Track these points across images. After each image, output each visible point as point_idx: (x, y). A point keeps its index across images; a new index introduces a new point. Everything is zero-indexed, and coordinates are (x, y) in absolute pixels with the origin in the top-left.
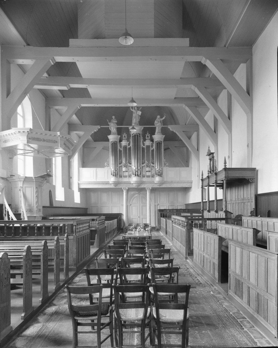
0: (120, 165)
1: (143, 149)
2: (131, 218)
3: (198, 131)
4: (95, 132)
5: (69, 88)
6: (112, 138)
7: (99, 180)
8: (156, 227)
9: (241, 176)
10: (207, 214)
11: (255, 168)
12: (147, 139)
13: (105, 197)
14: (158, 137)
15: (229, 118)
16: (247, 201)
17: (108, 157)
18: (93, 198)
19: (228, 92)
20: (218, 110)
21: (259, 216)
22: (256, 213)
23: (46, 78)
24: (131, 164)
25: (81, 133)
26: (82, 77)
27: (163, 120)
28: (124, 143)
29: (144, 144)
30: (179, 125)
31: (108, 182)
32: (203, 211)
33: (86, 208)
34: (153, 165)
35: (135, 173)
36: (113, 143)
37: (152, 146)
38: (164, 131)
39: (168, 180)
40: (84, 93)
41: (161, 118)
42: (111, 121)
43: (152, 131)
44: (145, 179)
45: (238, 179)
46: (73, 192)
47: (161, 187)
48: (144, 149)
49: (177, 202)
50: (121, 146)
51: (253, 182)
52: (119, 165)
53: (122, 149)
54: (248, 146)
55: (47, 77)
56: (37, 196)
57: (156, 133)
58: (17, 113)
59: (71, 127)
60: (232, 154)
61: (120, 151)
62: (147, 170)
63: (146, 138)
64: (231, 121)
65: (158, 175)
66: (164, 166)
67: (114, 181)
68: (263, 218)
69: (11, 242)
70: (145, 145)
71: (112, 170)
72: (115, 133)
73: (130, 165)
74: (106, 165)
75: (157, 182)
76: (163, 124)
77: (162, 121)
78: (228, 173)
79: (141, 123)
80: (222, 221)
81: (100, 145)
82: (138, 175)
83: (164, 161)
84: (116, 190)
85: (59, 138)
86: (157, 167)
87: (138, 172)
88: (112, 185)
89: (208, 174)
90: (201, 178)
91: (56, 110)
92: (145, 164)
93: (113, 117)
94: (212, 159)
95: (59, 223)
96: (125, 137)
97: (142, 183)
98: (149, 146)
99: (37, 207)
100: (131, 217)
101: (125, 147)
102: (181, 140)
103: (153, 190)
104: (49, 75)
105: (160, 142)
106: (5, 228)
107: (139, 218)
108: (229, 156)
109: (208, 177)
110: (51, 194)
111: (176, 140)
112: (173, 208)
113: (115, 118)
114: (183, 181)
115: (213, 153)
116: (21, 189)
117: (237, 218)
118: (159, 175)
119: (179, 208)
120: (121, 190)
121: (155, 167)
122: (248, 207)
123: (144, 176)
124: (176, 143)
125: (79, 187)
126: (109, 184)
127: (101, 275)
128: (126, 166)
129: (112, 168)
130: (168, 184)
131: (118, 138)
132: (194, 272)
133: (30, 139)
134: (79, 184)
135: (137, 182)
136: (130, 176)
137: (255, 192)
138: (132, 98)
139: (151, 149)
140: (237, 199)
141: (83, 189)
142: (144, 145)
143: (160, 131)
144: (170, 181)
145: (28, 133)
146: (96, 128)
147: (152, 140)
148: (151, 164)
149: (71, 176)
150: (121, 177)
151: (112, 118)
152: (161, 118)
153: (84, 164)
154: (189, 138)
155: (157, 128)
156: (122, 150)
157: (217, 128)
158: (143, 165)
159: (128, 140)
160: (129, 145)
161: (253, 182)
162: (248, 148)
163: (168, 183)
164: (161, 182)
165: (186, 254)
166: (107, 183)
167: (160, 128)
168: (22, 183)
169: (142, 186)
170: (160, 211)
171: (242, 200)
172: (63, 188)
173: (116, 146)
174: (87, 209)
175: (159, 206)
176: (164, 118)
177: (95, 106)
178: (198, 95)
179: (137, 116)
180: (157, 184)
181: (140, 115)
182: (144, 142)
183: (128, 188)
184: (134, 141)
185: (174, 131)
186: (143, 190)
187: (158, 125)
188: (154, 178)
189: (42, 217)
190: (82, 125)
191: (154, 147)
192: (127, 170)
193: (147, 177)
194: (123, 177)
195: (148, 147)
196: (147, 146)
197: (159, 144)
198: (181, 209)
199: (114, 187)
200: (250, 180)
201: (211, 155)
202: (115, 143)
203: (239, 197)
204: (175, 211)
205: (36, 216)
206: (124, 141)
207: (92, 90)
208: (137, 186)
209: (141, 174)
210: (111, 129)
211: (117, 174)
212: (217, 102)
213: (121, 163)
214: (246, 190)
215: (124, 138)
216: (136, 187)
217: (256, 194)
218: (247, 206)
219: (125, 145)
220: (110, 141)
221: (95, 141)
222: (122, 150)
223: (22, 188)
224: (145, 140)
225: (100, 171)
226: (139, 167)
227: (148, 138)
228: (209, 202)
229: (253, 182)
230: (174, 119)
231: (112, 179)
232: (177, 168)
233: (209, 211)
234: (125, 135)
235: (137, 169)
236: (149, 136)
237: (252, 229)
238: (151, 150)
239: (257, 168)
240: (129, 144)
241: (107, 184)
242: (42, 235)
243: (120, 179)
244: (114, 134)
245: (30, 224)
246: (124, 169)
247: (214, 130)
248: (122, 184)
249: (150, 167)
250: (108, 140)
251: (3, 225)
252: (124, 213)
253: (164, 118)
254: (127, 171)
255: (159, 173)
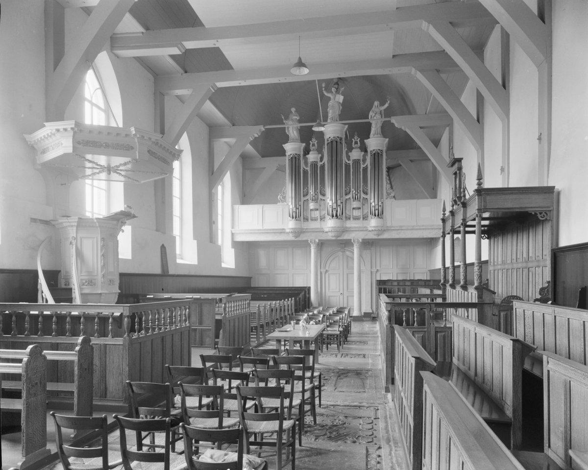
0: (306, 198)
1: (347, 166)
2: (327, 298)
3: (450, 124)
4: (256, 138)
5: (184, 51)
6: (291, 148)
7: (268, 226)
8: (373, 313)
9: (517, 206)
10: (452, 291)
11: (554, 187)
12: (355, 148)
13: (281, 258)
14: (375, 142)
15: (505, 85)
16: (535, 264)
17: (284, 184)
18: (263, 259)
19: (502, 26)
20: (485, 75)
21: (550, 302)
22: (554, 294)
23: (141, 35)
24: (324, 195)
25: (232, 141)
26: (204, 26)
27: (385, 110)
28: (312, 157)
29: (348, 158)
30: (417, 114)
31: (283, 229)
32: (444, 285)
33: (248, 276)
34: (365, 196)
35: (332, 211)
36: (292, 158)
37: (364, 160)
38: (387, 130)
39: (393, 225)
40: (215, 61)
41: (380, 106)
42: (288, 117)
43: (364, 131)
44: (351, 224)
45: (516, 216)
46: (219, 250)
47: (379, 237)
48: (350, 166)
49: (293, 267)
50: (306, 163)
51: (548, 218)
52: (303, 199)
53: (308, 169)
54: (540, 139)
55: (143, 33)
56: (103, 255)
57: (371, 135)
58: (82, 99)
59: (214, 131)
60: (503, 161)
61: (305, 172)
62: (355, 206)
63: (353, 146)
64: (509, 90)
65: (375, 216)
66: (387, 199)
67: (293, 227)
68: (557, 309)
69: (4, 352)
70: (352, 159)
71: (291, 207)
72: (297, 140)
73: (323, 198)
74: (280, 198)
75: (373, 229)
76: (384, 116)
77: (383, 112)
78: (485, 201)
79: (342, 117)
80: (470, 309)
81: (271, 164)
82: (336, 215)
83: (386, 189)
84: (298, 244)
85: (136, 140)
86: (373, 202)
87: (337, 211)
88: (291, 234)
89: (453, 206)
90: (442, 216)
91: (177, 96)
92: (350, 196)
93: (293, 110)
94: (458, 172)
95: (113, 311)
96: (313, 145)
97: (345, 230)
98: (359, 160)
99: (103, 276)
100: (328, 294)
101: (314, 165)
102: (420, 148)
103: (367, 244)
104: (147, 29)
105: (379, 151)
106: (14, 318)
107: (341, 297)
108: (502, 167)
109: (452, 213)
110: (166, 253)
111: (412, 149)
112: (405, 279)
113: (295, 112)
114: (423, 226)
115: (459, 160)
116: (74, 242)
117: (504, 303)
118: (377, 215)
119: (416, 278)
120: (306, 245)
121: (369, 200)
122: (537, 279)
123: (348, 218)
124: (413, 154)
125: (233, 238)
126: (284, 232)
127: (266, 399)
128: (315, 200)
129: (290, 204)
130: (394, 232)
131: (302, 148)
132: (384, 431)
133: (79, 143)
134: (233, 234)
135: (334, 229)
136: (322, 218)
137: (552, 244)
138: (300, 59)
139: (362, 166)
140: (515, 261)
141: (243, 243)
142: (349, 160)
143: (379, 130)
144: (397, 227)
145: (75, 133)
146: (257, 131)
147: (364, 149)
148: (363, 195)
149: (214, 219)
150: (306, 219)
151: (291, 112)
152: (380, 106)
153: (245, 196)
154: (436, 143)
155: (373, 125)
156: (309, 171)
157: (483, 113)
158: (347, 197)
159: (320, 150)
160: (321, 161)
161: (546, 219)
162: (540, 143)
163: (393, 230)
164: (380, 228)
165: (387, 380)
166: (282, 231)
167: (380, 125)
168: (75, 231)
169: (346, 237)
170: (381, 283)
171: (526, 262)
172: (196, 241)
173: (297, 165)
174: (251, 278)
175: (378, 275)
176: (386, 105)
177: (242, 85)
178: (442, 47)
179: (336, 105)
180: (373, 232)
181: (341, 102)
182: (350, 154)
183: (319, 240)
184: (330, 154)
185: (403, 128)
186: (348, 244)
187: (375, 120)
188: (366, 221)
189: (118, 294)
190: (233, 126)
191: (368, 162)
192: (317, 207)
193: (354, 219)
194: (310, 220)
195: (357, 162)
196: (354, 160)
197: (377, 156)
198: (421, 280)
199: (293, 239)
200: (539, 216)
201: (456, 165)
202: (296, 157)
203: (518, 254)
204: (409, 284)
205: (101, 294)
206: (312, 154)
207: (234, 51)
208: (335, 236)
209: (342, 214)
210: (289, 131)
211: (299, 215)
212: (482, 60)
213: (306, 195)
214: (533, 240)
215: (312, 148)
216: (334, 238)
217: (554, 247)
218: (534, 276)
219: (313, 160)
220: (288, 154)
221: (264, 155)
222: (309, 171)
223: (76, 239)
224: (350, 149)
225: (269, 209)
226: (339, 202)
227: (356, 145)
228: (466, 266)
229: (546, 219)
230: (407, 106)
231: (291, 224)
232: (414, 201)
233: (464, 288)
234: (314, 141)
235: (335, 204)
236: (359, 142)
237: (512, 342)
238: (362, 168)
239: (558, 187)
240: (322, 159)
241: (281, 232)
242: (65, 335)
243: (306, 223)
244: (294, 141)
245: (56, 310)
246: (312, 205)
247: (476, 119)
248: (309, 233)
249: (360, 201)
250: (283, 153)
251: (37, 313)
252: (312, 286)
253: (386, 105)
254: (317, 210)
255: (377, 212)
